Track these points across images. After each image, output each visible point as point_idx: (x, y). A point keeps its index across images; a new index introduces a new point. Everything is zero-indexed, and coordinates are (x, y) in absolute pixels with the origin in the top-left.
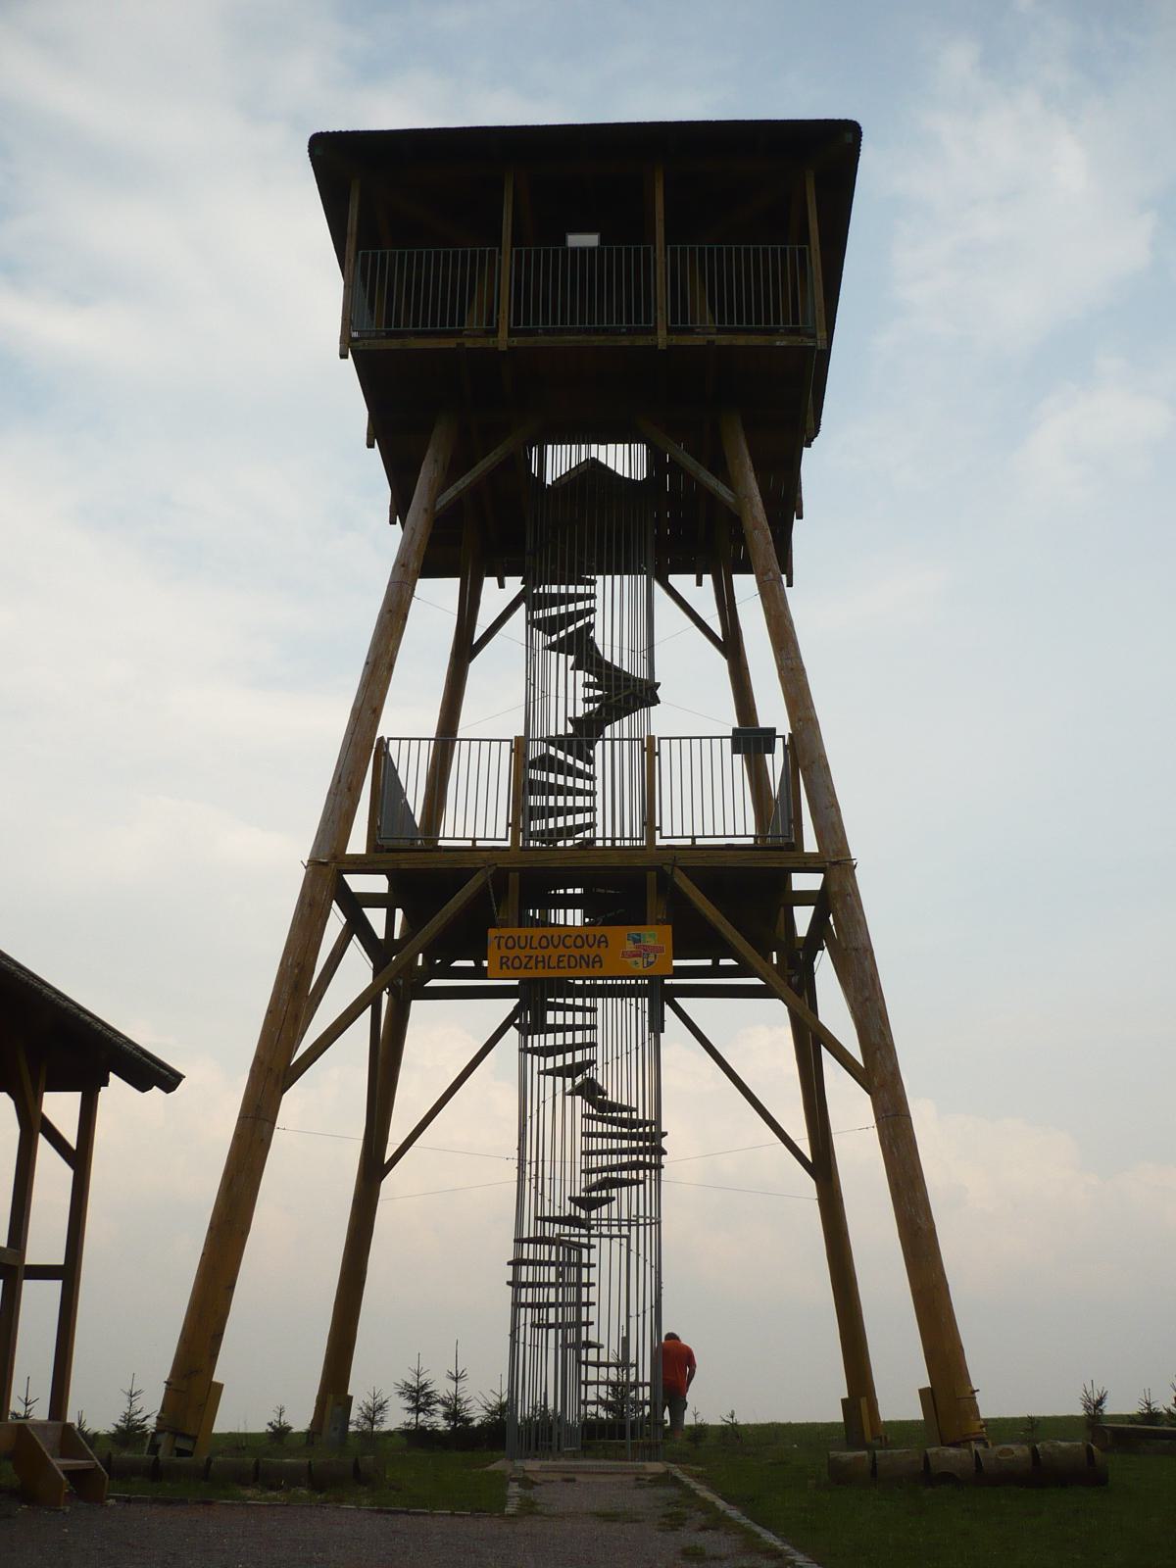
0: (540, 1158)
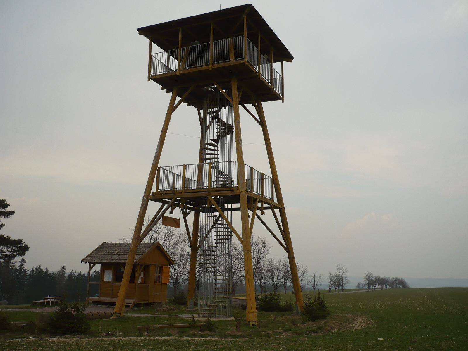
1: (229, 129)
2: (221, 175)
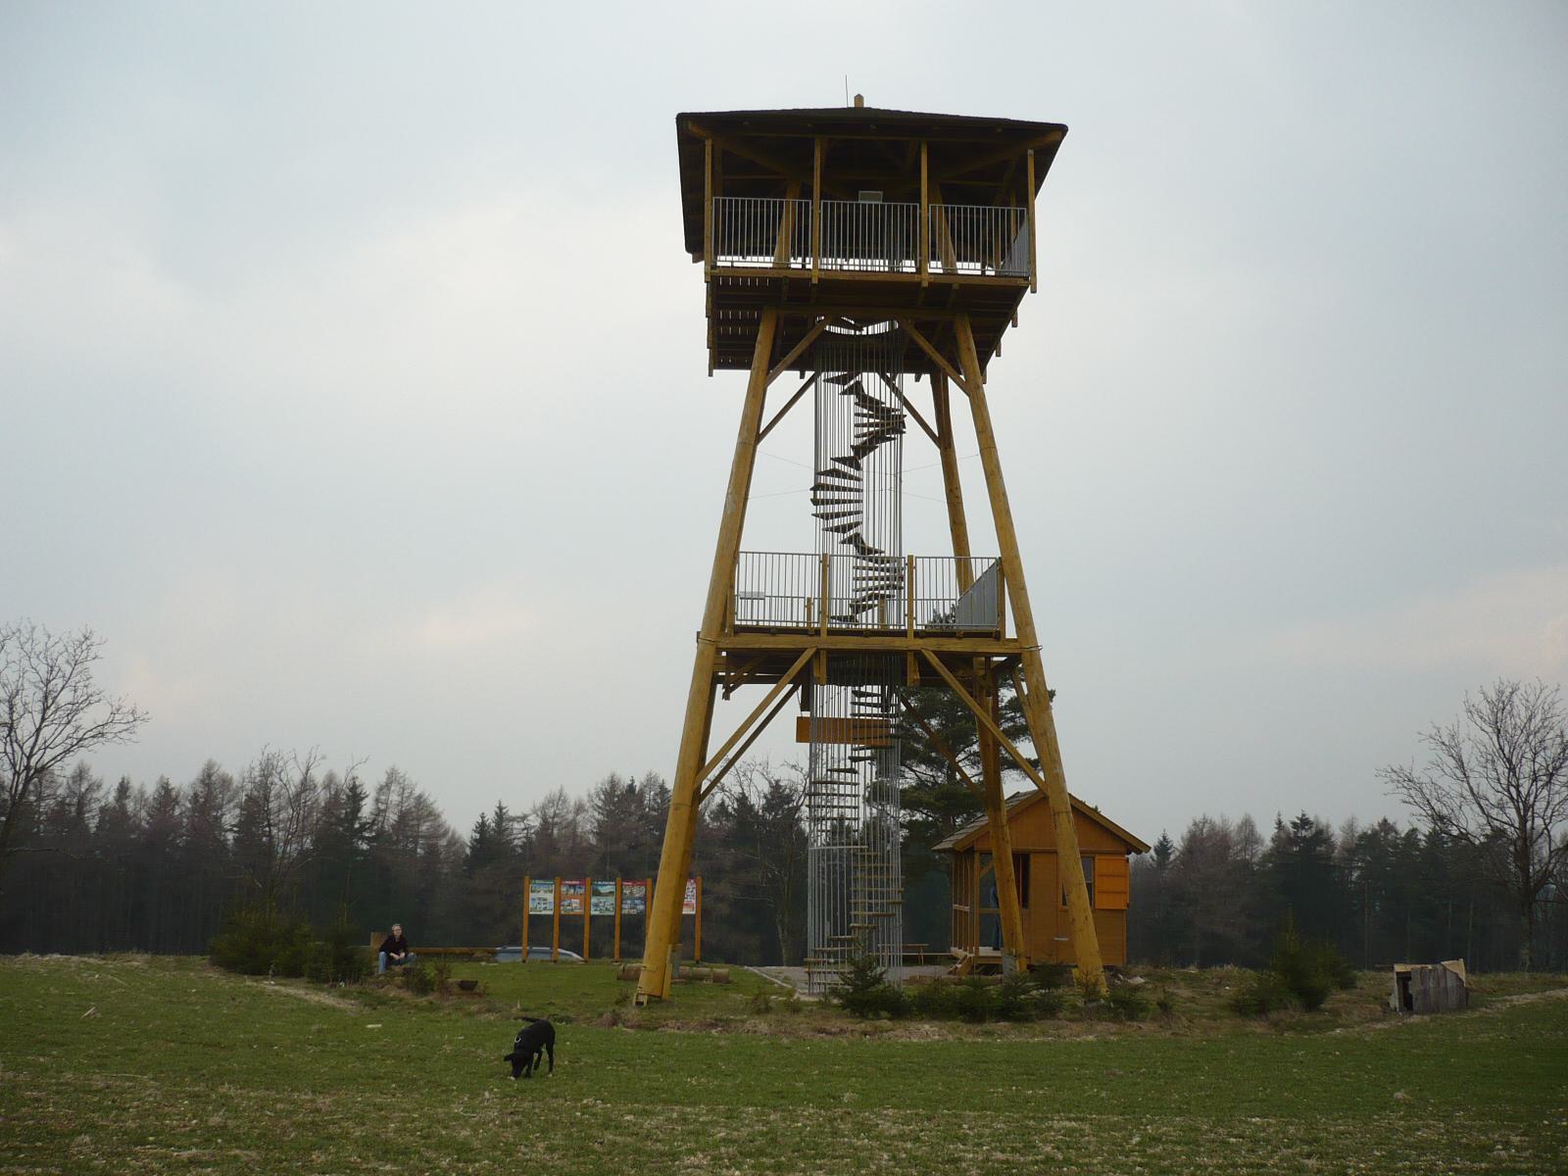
1: (888, 424)
2: (876, 562)
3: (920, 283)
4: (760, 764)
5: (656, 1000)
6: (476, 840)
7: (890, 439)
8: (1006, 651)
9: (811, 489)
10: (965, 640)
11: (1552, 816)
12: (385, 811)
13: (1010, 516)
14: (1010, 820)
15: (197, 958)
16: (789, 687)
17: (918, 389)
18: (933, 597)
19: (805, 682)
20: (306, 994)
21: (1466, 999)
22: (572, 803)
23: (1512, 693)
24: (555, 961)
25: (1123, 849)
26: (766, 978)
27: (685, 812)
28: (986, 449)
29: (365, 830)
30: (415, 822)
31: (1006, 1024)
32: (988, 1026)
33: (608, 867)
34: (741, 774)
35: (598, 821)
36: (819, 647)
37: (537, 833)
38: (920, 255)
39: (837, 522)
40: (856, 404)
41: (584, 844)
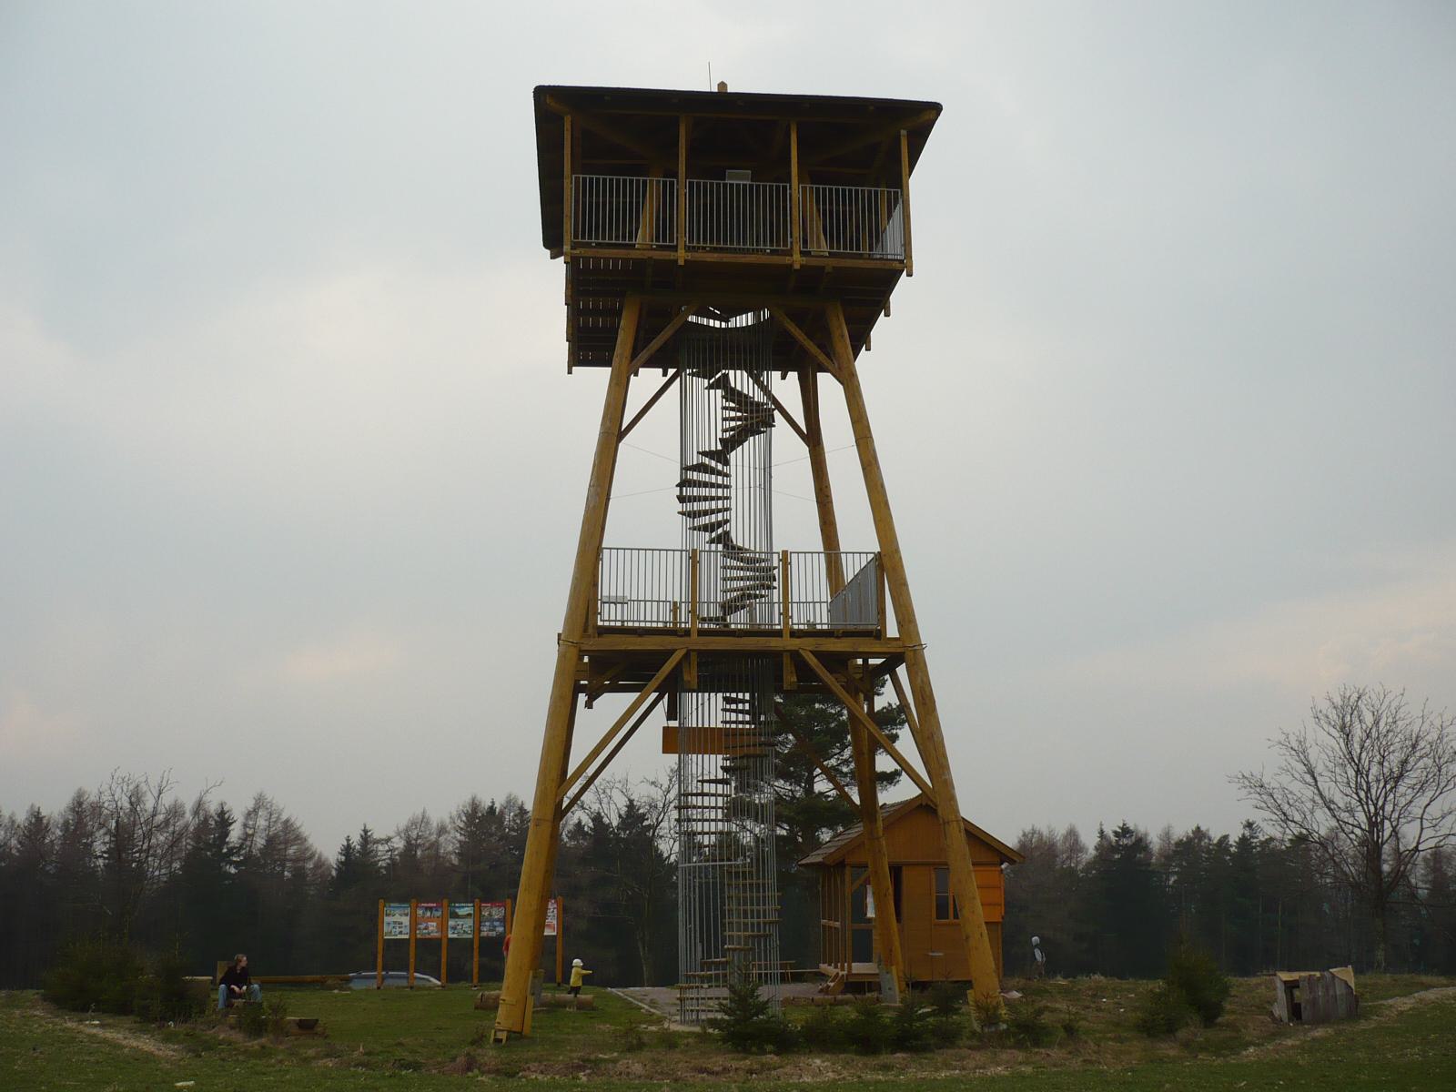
0: (752, 489)
1: (757, 417)
3: (791, 265)
4: (620, 782)
5: (516, 1036)
6: (342, 862)
7: (763, 432)
8: (884, 650)
9: (677, 486)
10: (844, 640)
11: (1399, 817)
12: (253, 835)
13: (889, 509)
14: (885, 829)
15: (31, 994)
16: (654, 695)
17: (786, 388)
18: (810, 600)
19: (673, 689)
20: (125, 1038)
21: (1355, 1008)
22: (435, 825)
23: (1359, 698)
24: (411, 988)
25: (997, 859)
26: (631, 1003)
27: (546, 829)
28: (861, 438)
29: (233, 855)
30: (282, 846)
31: (904, 1055)
32: (885, 1058)
33: (469, 887)
34: (601, 791)
35: (460, 842)
36: (691, 648)
37: (400, 855)
38: (791, 237)
39: (705, 520)
40: (723, 397)
41: (447, 864)
